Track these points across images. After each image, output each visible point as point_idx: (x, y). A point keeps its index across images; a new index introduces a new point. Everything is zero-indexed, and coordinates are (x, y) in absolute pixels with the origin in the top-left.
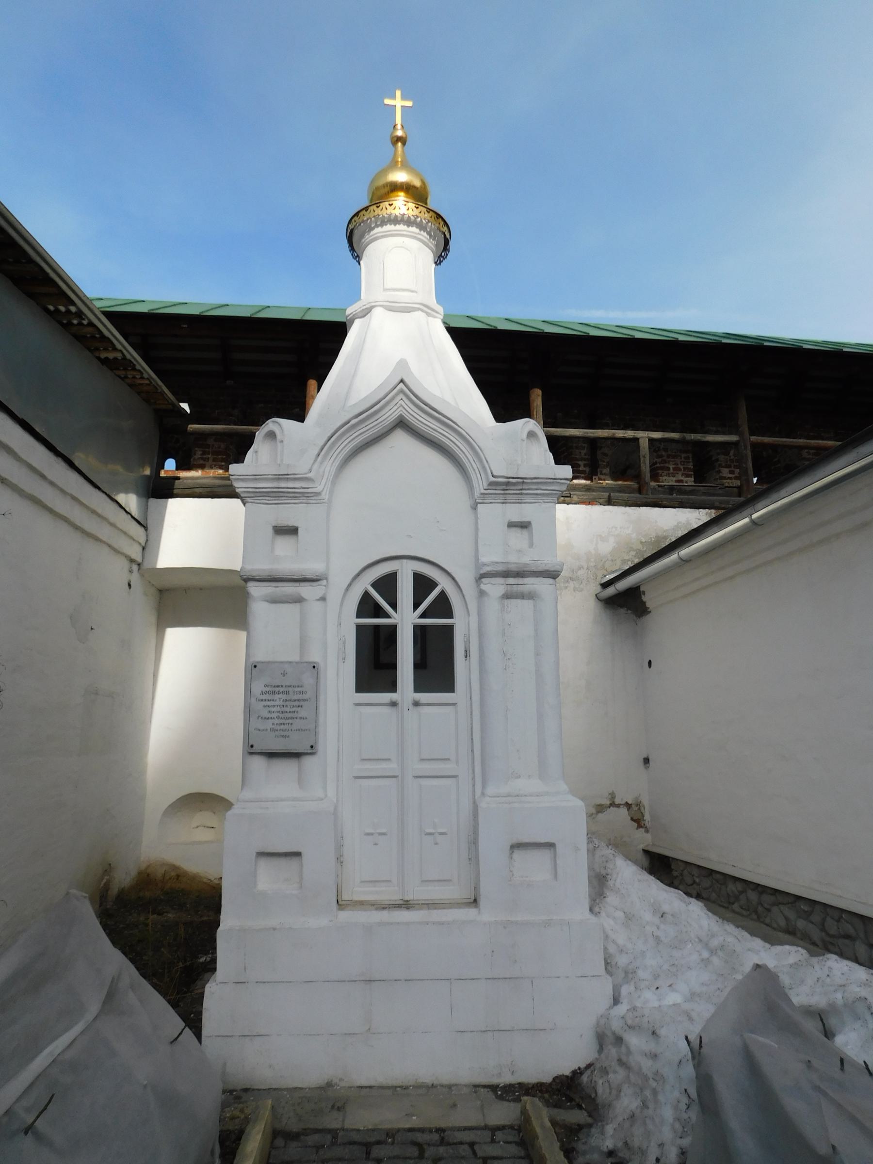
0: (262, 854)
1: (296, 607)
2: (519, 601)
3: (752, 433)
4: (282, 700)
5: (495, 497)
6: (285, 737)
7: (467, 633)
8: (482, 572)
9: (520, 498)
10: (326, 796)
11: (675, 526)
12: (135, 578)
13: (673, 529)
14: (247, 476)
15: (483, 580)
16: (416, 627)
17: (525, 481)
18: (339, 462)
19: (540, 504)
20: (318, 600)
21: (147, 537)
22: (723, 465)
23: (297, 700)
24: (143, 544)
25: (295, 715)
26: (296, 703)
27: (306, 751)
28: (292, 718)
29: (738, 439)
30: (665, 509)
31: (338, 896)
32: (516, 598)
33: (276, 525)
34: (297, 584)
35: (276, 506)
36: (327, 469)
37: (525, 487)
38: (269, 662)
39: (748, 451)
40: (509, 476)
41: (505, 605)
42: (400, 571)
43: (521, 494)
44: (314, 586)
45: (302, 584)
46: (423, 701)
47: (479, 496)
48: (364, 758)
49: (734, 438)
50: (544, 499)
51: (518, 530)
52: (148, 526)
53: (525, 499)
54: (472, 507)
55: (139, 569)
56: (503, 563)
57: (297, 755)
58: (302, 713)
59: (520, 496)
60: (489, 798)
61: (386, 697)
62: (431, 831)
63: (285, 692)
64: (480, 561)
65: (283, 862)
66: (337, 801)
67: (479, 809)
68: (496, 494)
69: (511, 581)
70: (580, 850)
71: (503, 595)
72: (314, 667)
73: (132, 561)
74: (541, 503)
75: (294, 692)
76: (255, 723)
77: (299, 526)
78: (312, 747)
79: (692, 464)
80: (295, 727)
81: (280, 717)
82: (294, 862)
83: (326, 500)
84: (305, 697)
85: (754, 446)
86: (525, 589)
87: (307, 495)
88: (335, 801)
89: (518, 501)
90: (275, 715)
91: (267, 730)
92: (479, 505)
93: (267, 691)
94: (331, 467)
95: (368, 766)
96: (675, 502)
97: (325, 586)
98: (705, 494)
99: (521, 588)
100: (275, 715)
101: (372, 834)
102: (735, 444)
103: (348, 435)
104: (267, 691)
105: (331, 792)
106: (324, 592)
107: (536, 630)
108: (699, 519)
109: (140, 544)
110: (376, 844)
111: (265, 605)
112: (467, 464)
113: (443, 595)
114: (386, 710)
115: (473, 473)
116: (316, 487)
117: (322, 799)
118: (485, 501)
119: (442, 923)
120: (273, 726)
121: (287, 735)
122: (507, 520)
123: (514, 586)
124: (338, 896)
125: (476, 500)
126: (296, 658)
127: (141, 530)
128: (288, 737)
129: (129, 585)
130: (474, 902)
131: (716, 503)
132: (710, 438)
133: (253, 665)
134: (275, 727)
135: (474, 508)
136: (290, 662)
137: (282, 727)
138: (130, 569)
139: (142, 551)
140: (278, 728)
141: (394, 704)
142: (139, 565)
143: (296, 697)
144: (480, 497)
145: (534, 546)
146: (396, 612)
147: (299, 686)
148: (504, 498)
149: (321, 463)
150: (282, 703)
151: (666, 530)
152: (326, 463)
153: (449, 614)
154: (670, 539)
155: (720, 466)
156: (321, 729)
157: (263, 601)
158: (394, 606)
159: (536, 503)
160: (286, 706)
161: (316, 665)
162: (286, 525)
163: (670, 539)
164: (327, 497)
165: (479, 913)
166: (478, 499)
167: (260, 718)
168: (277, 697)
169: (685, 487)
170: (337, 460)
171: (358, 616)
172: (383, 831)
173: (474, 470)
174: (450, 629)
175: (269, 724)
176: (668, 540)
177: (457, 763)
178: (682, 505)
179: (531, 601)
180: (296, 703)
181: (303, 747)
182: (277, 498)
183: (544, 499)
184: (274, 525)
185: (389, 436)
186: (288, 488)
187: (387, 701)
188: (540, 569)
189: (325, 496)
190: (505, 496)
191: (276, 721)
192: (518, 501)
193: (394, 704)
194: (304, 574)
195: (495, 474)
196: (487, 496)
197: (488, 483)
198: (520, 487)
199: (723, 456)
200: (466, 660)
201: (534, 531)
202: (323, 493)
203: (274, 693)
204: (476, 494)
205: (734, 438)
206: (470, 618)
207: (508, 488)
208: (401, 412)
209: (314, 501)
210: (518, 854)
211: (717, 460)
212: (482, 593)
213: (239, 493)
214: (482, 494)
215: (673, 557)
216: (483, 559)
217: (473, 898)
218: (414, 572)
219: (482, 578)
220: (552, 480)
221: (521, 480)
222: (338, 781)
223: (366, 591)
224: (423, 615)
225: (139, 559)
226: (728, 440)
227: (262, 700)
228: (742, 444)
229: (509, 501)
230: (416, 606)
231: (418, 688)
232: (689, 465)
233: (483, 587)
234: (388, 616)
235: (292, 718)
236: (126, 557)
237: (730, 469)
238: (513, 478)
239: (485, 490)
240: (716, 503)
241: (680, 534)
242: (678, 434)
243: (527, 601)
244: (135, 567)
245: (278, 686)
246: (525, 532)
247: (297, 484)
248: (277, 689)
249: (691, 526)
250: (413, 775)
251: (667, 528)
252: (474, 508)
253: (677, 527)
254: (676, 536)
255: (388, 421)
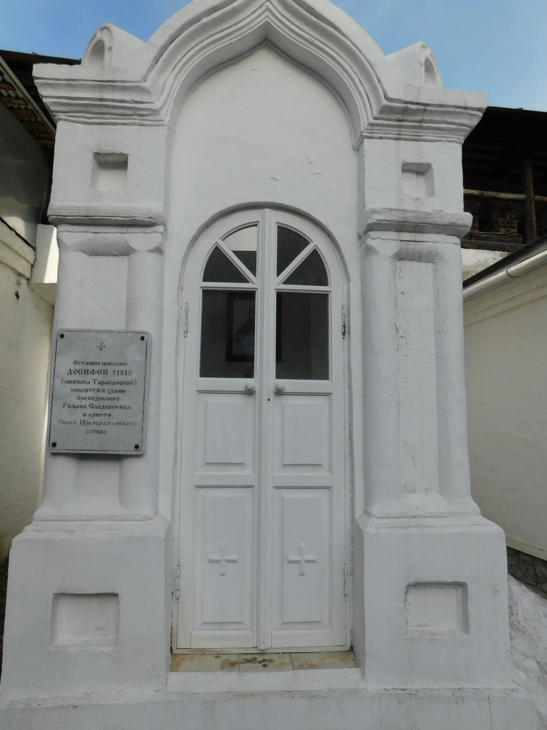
0: (59, 596)
1: (120, 263)
2: (414, 264)
3: (536, 193)
4: (97, 382)
5: (388, 130)
6: (99, 432)
7: (345, 304)
8: (370, 222)
9: (418, 134)
10: (156, 513)
11: (476, 263)
12: (23, 290)
13: (474, 266)
14: (58, 80)
15: (370, 233)
16: (281, 297)
17: (428, 108)
18: (184, 77)
19: (443, 143)
20: (151, 251)
21: (35, 257)
22: (502, 225)
23: (118, 383)
24: (32, 263)
25: (114, 403)
26: (118, 387)
27: (128, 453)
28: (110, 407)
29: (525, 197)
30: (467, 249)
31: (171, 642)
32: (411, 260)
33: (98, 152)
34: (124, 230)
35: (99, 127)
36: (170, 82)
37: (427, 117)
38: (80, 331)
39: (533, 207)
40: (408, 100)
41: (398, 269)
42: (261, 222)
43: (420, 128)
44: (146, 233)
45: (131, 230)
46: (288, 389)
47: (366, 126)
48: (209, 462)
49: (522, 196)
50: (448, 137)
51: (413, 176)
52: (37, 248)
53: (424, 136)
54: (354, 148)
55: (28, 284)
56: (398, 210)
57: (118, 458)
58: (124, 401)
59: (418, 130)
60: (375, 519)
61: (240, 383)
62: (297, 558)
63: (102, 372)
64: (367, 209)
65: (95, 604)
66: (173, 518)
67: (365, 535)
68: (388, 126)
69: (406, 236)
70: (499, 592)
71: (397, 253)
72: (143, 338)
73: (20, 275)
74: (444, 142)
75: (114, 372)
76: (66, 415)
77: (129, 153)
78: (137, 447)
79: (478, 224)
80: (114, 420)
81: (94, 406)
82: (109, 605)
83: (165, 122)
84: (128, 378)
85: (538, 203)
86: (424, 247)
87: (139, 112)
88: (169, 518)
89: (415, 137)
90: (87, 403)
91: (75, 422)
92: (366, 141)
93: (78, 370)
94: (174, 81)
95: (214, 472)
96: (474, 246)
97: (162, 233)
98: (496, 240)
99: (418, 246)
100: (87, 403)
101: (218, 561)
102: (523, 201)
103: (198, 40)
104: (78, 370)
105: (164, 508)
106: (160, 241)
107: (437, 301)
108: (495, 259)
109: (28, 261)
110: (223, 575)
111: (82, 257)
112: (351, 89)
113: (315, 255)
114: (240, 400)
115: (359, 98)
116: (152, 103)
117: (150, 519)
118: (374, 135)
119: (311, 695)
120: (85, 418)
121: (103, 431)
122: (402, 161)
123: (410, 243)
124: (171, 642)
125: (362, 132)
126: (122, 327)
127: (29, 250)
128: (105, 432)
129: (17, 296)
130: (350, 650)
131: (507, 247)
132: (503, 195)
133: (60, 334)
134: (86, 418)
135: (358, 149)
136: (111, 332)
137: (96, 419)
138: (18, 282)
139: (31, 268)
140: (91, 420)
141: (250, 392)
142: (28, 280)
143: (116, 378)
144: (368, 129)
145: (435, 194)
146: (255, 276)
147: (120, 364)
148: (397, 133)
149: (161, 71)
150: (97, 386)
151: (469, 266)
152: (167, 74)
153: (323, 280)
154: (472, 274)
155: (499, 226)
156: (151, 424)
157: (78, 250)
158: (253, 270)
159: (437, 141)
160: (103, 391)
161: (144, 336)
162: (110, 152)
163: (472, 274)
164: (167, 119)
165: (363, 673)
166: (365, 132)
167: (66, 407)
168: (90, 377)
169: (482, 235)
170: (182, 73)
171: (205, 279)
172: (234, 557)
173: (361, 94)
174: (324, 298)
175: (78, 416)
176: (469, 275)
177: (331, 470)
178: (480, 247)
179: (430, 265)
180: (118, 387)
181: (126, 448)
182: (100, 116)
183: (448, 137)
184: (95, 151)
185: (250, 57)
186: (114, 101)
187: (241, 388)
188: (445, 221)
189: (165, 116)
190: (399, 129)
191: (89, 411)
192: (415, 137)
193: (250, 392)
194: (132, 215)
195: (390, 95)
196: (377, 128)
197: (380, 108)
198: (419, 118)
199: (502, 219)
200: (344, 338)
201: (435, 176)
202: (163, 112)
203: (87, 372)
204: (362, 125)
205: (522, 196)
206: (351, 284)
207: (405, 118)
208: (267, 19)
209: (149, 123)
210: (413, 595)
211: (497, 222)
212: (368, 251)
213: (48, 104)
214: (371, 125)
215: (502, 274)
216: (369, 206)
217: (349, 645)
218: (279, 225)
219: (368, 231)
220: (461, 110)
221: (422, 107)
222: (174, 490)
223: (217, 247)
224: (288, 281)
225: (28, 274)
226: (517, 198)
227: (70, 382)
228: (529, 202)
229: (404, 137)
230: (280, 270)
231: (280, 374)
232: (475, 225)
233: (370, 242)
234: (244, 280)
235: (110, 407)
236: (12, 269)
237: (507, 229)
238: (412, 103)
239: (375, 119)
240: (507, 247)
241: (479, 270)
242: (478, 191)
243: (425, 264)
244: (24, 282)
245: (93, 364)
246: (422, 180)
247: (127, 96)
248: (90, 368)
249: (489, 264)
250: (273, 486)
251: (469, 265)
252: (358, 149)
253: (477, 265)
254: (477, 271)
255: (251, 28)
